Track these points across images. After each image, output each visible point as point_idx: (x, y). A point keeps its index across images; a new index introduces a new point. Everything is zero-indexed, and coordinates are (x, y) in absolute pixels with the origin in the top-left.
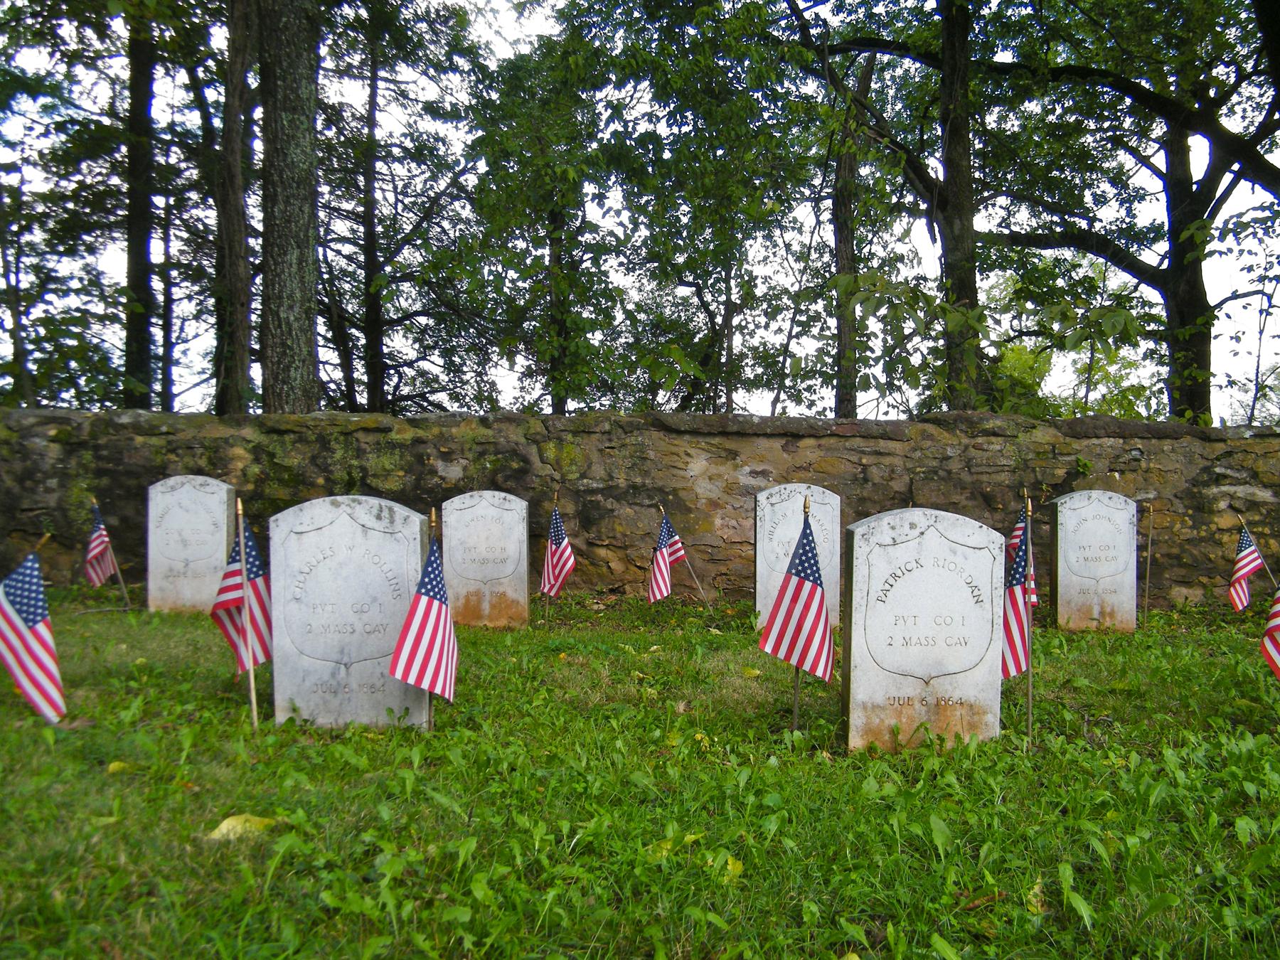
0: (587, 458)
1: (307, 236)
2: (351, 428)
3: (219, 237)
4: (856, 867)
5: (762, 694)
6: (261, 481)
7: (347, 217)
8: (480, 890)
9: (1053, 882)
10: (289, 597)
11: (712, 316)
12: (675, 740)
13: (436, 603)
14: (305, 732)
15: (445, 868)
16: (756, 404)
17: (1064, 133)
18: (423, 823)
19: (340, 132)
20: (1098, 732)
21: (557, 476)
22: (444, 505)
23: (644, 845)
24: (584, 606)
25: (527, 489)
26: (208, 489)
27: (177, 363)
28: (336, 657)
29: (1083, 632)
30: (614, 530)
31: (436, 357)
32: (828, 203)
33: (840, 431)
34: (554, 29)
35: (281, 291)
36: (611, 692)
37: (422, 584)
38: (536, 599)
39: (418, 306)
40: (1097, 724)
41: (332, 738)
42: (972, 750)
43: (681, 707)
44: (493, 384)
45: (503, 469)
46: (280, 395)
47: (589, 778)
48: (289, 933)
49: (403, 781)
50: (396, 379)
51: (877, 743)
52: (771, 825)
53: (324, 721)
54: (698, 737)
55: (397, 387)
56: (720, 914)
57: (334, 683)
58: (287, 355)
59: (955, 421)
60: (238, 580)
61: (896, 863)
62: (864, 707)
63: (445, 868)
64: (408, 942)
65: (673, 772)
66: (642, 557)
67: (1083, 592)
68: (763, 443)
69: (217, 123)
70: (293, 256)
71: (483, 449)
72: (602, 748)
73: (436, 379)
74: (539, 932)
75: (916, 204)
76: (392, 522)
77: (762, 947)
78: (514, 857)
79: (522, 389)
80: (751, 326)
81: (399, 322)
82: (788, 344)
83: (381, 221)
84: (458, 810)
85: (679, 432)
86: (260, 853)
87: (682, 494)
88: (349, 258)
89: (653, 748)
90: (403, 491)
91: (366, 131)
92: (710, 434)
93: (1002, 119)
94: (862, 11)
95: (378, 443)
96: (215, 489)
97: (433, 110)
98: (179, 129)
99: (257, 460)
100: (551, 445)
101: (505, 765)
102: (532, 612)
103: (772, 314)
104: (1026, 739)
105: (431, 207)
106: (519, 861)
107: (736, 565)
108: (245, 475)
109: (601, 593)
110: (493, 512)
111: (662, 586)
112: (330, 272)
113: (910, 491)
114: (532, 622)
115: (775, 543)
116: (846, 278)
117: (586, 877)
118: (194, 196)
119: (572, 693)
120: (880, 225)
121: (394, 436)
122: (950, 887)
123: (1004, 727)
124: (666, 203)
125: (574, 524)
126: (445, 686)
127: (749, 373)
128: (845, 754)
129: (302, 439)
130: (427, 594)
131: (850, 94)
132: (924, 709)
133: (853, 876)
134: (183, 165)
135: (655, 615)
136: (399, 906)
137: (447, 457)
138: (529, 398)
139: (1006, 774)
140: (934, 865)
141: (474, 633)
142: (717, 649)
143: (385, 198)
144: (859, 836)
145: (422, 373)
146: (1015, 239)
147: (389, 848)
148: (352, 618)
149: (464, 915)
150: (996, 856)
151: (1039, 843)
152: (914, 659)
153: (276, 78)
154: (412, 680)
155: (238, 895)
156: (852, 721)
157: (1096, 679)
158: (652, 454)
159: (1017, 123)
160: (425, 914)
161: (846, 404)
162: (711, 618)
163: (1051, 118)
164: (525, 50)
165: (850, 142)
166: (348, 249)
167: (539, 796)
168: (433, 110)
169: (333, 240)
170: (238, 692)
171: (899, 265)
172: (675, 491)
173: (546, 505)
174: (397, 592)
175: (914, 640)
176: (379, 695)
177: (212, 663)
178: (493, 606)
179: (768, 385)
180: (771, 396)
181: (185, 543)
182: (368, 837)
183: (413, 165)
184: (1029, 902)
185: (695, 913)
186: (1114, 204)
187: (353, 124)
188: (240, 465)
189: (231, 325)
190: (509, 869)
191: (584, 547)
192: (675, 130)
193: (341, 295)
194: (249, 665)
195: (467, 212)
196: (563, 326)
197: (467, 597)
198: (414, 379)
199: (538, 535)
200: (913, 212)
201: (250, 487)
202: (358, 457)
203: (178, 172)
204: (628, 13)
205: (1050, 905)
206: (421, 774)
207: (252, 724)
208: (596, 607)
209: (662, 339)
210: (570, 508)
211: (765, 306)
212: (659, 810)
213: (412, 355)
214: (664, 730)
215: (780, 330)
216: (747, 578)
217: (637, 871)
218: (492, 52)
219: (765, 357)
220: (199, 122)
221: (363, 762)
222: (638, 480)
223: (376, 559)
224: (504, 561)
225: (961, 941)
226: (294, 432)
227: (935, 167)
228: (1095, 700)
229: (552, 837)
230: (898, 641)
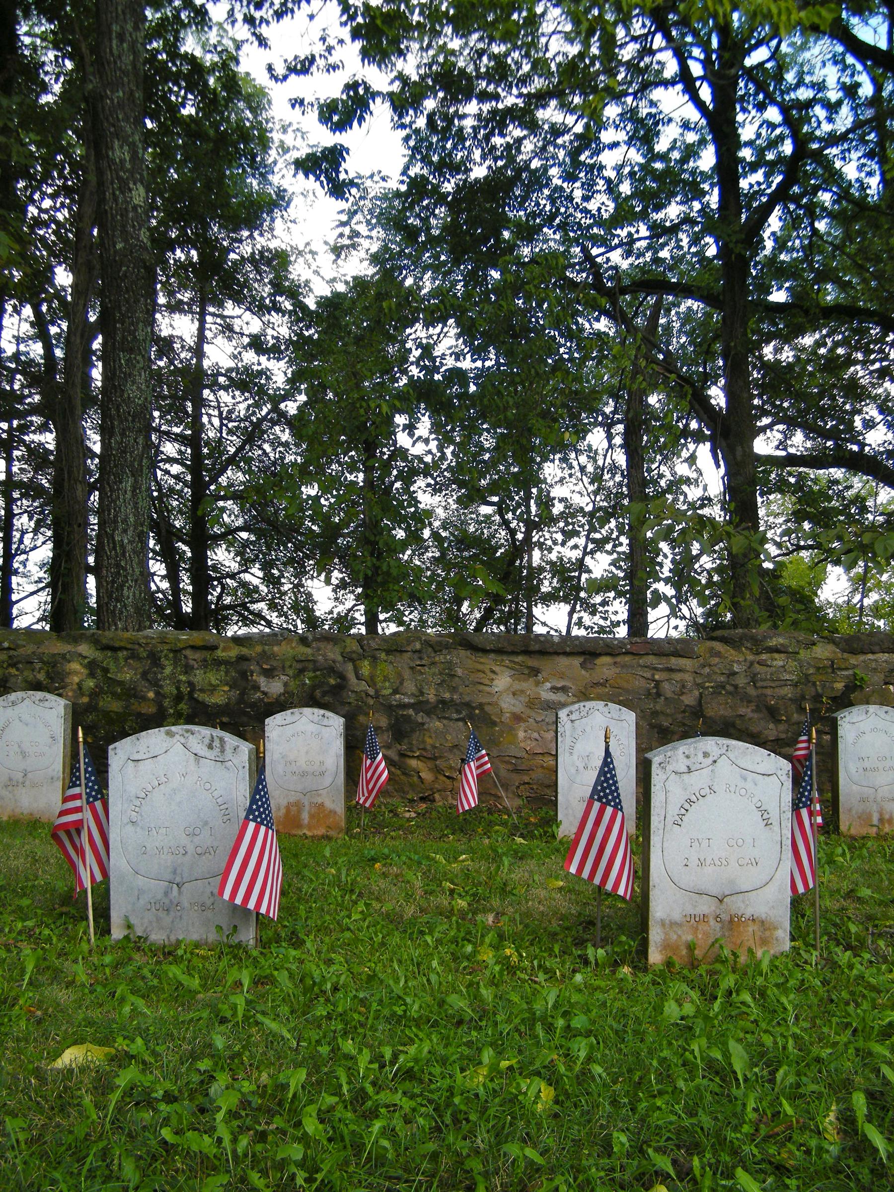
0: (399, 675)
1: (140, 465)
2: (180, 645)
3: (57, 457)
4: (661, 1093)
5: (563, 904)
6: (94, 695)
7: (175, 440)
8: (311, 1125)
9: (848, 1109)
10: (126, 820)
11: (513, 532)
12: (487, 956)
13: (263, 829)
14: (139, 949)
15: (275, 1100)
16: (552, 618)
17: (834, 365)
18: (254, 1050)
19: (171, 362)
20: (881, 943)
21: (371, 692)
22: (267, 721)
23: (462, 1070)
24: (396, 815)
25: (343, 704)
26: (47, 704)
27: (16, 572)
28: (168, 877)
29: (863, 838)
30: (424, 742)
31: (256, 570)
32: (620, 428)
33: (634, 649)
34: (368, 270)
35: (116, 516)
36: (423, 903)
37: (250, 811)
38: (352, 809)
39: (240, 522)
40: (880, 935)
41: (164, 954)
42: (765, 966)
43: (490, 918)
44: (309, 595)
45: (321, 685)
46: (113, 612)
47: (408, 1000)
48: (129, 1171)
49: (236, 1005)
50: (219, 590)
51: (675, 958)
52: (581, 1048)
53: (157, 937)
54: (508, 952)
55: (220, 597)
56: (535, 1146)
57: (167, 901)
58: (119, 573)
59: (741, 639)
60: (78, 803)
61: (698, 1088)
62: (663, 923)
63: (275, 1100)
64: (243, 1180)
65: (487, 993)
66: (451, 768)
67: (863, 800)
68: (563, 661)
69: (59, 353)
70: (128, 484)
71: (302, 666)
72: (419, 965)
73: (256, 589)
74: (366, 1163)
75: (700, 430)
76: (223, 751)
77: (575, 1179)
78: (341, 1086)
79: (336, 599)
80: (549, 543)
81: (223, 536)
82: (583, 559)
83: (207, 444)
84: (288, 1036)
85: (485, 651)
86: (102, 1085)
87: (487, 708)
88: (177, 477)
89: (465, 964)
90: (227, 704)
91: (194, 361)
92: (513, 653)
93: (778, 350)
94: (649, 255)
95: (205, 660)
96: (53, 704)
97: (257, 344)
98: (23, 358)
99: (92, 675)
100: (366, 663)
101: (329, 986)
102: (349, 820)
103: (569, 535)
104: (815, 953)
105: (253, 431)
106: (345, 1088)
107: (537, 775)
108: (80, 688)
109: (412, 801)
110: (312, 728)
111: (470, 798)
112: (159, 490)
113: (700, 704)
114: (348, 831)
115: (575, 757)
116: (637, 500)
117: (407, 1105)
118: (36, 420)
119: (388, 907)
120: (669, 452)
121: (220, 653)
122: (751, 1115)
123: (793, 939)
124: (471, 430)
125: (387, 737)
126: (270, 907)
127: (545, 588)
128: (645, 970)
129: (134, 656)
130: (254, 820)
131: (640, 335)
132: (719, 925)
133: (659, 1103)
134: (26, 392)
135: (464, 824)
136: (235, 1140)
137: (269, 674)
138: (341, 609)
139: (798, 990)
140: (734, 1090)
141: (296, 850)
142: (521, 859)
143: (211, 422)
144: (663, 1061)
145: (244, 584)
146: (792, 460)
147: (223, 1079)
148: (184, 840)
149: (296, 1151)
150: (792, 1079)
151: (832, 1066)
152: (710, 878)
153: (115, 322)
154: (238, 901)
155: (80, 1131)
156: (651, 937)
157: (877, 889)
158: (459, 672)
159: (791, 354)
160: (259, 1147)
161: (637, 621)
162: (516, 827)
163: (822, 351)
164: (341, 288)
165: (640, 378)
166: (176, 469)
167: (362, 1019)
168: (257, 344)
169: (162, 460)
170: (78, 908)
171: (685, 488)
172: (481, 706)
173: (362, 719)
174: (227, 817)
175: (708, 862)
176: (209, 914)
177: (49, 876)
178: (312, 816)
179: (565, 600)
180: (565, 608)
181: (24, 755)
182: (204, 1065)
183: (237, 393)
184: (825, 1129)
185: (513, 1149)
186: (882, 428)
187: (183, 355)
188: (76, 679)
189: (68, 544)
190: (337, 1099)
191: (396, 758)
192: (479, 364)
193: (168, 511)
194: (88, 884)
195: (286, 436)
196: (375, 542)
197: (288, 808)
198: (236, 590)
199: (355, 747)
200: (698, 437)
201: (85, 700)
202: (186, 673)
203: (21, 399)
204: (436, 257)
205: (845, 1132)
206: (250, 997)
207: (89, 941)
208: (407, 815)
209: (466, 554)
210: (384, 722)
211: (562, 524)
212: (474, 1033)
213: (234, 566)
214: (474, 944)
215: (576, 547)
216: (548, 786)
217: (457, 1100)
218: (311, 290)
219: (559, 569)
220: (41, 352)
221: (195, 983)
222: (447, 695)
223: (208, 786)
224: (322, 774)
225: (761, 1171)
226: (126, 649)
227: (717, 396)
228: (878, 910)
229: (376, 1066)
230: (694, 862)
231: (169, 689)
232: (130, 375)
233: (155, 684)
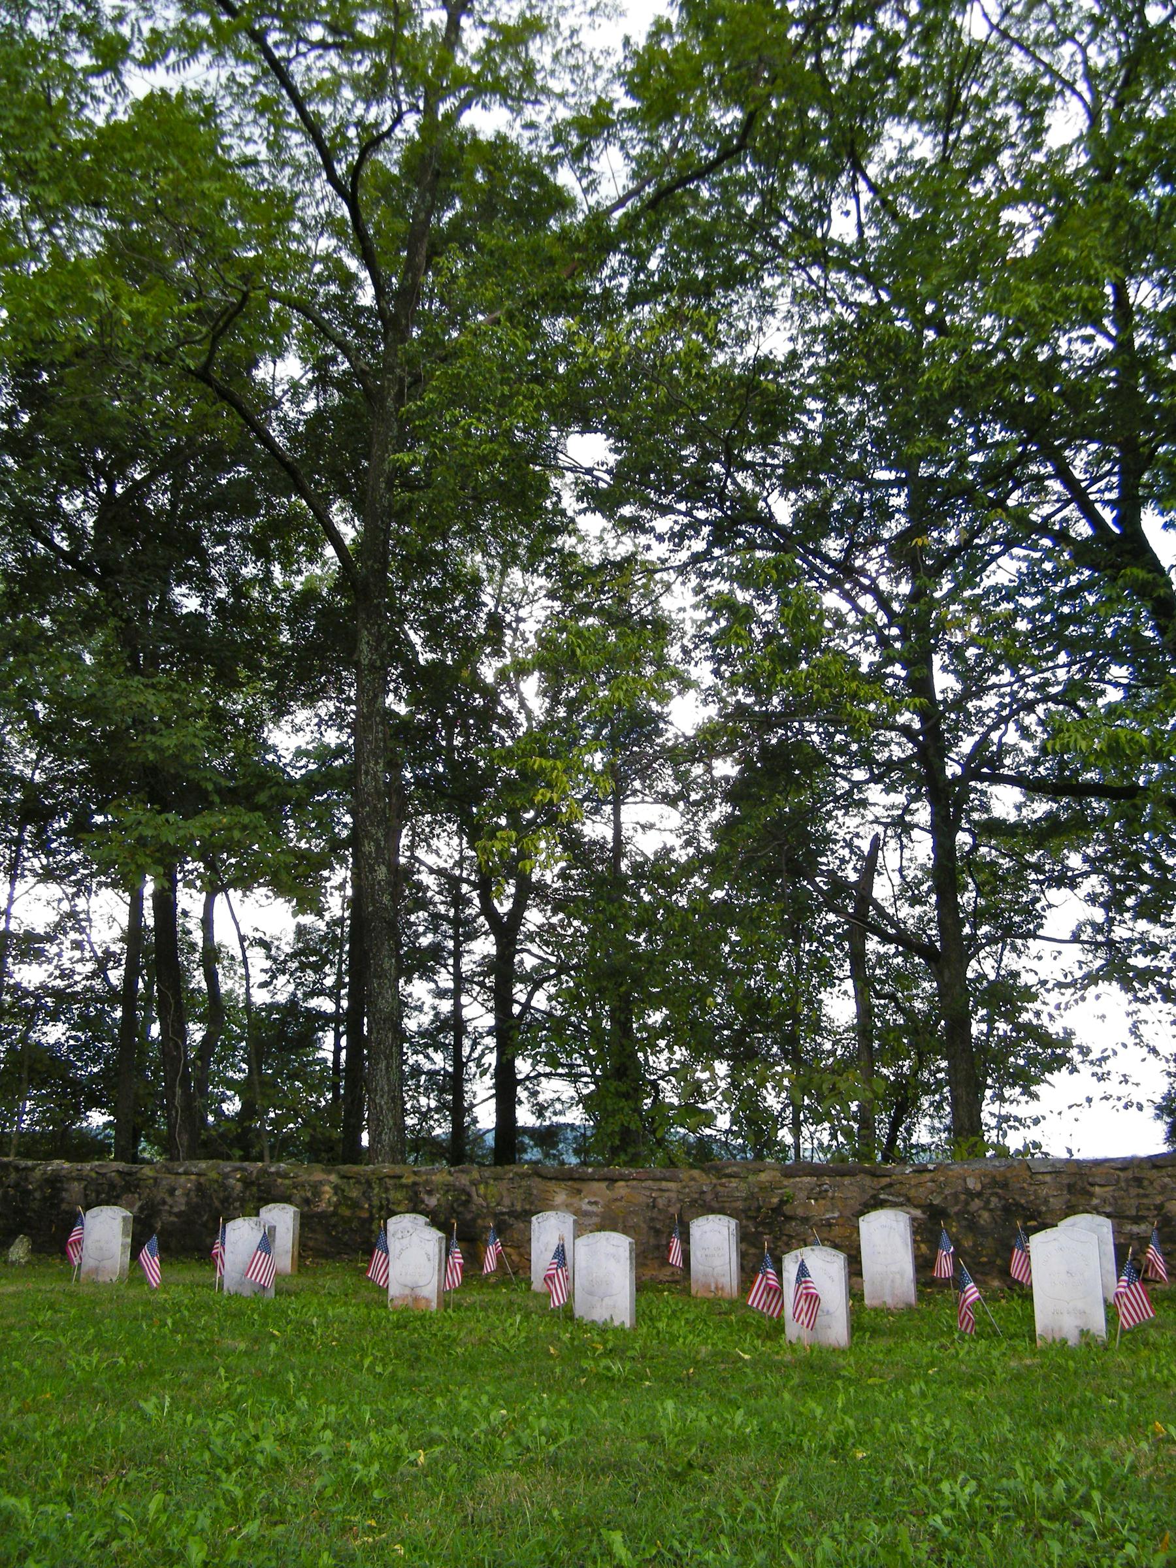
68: (595, 1185)
129: (358, 1182)
152: (409, 1281)
231: (376, 1202)
232: (1113, 579)
233: (369, 1199)
